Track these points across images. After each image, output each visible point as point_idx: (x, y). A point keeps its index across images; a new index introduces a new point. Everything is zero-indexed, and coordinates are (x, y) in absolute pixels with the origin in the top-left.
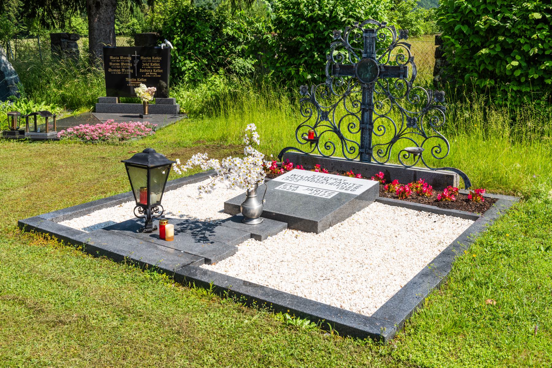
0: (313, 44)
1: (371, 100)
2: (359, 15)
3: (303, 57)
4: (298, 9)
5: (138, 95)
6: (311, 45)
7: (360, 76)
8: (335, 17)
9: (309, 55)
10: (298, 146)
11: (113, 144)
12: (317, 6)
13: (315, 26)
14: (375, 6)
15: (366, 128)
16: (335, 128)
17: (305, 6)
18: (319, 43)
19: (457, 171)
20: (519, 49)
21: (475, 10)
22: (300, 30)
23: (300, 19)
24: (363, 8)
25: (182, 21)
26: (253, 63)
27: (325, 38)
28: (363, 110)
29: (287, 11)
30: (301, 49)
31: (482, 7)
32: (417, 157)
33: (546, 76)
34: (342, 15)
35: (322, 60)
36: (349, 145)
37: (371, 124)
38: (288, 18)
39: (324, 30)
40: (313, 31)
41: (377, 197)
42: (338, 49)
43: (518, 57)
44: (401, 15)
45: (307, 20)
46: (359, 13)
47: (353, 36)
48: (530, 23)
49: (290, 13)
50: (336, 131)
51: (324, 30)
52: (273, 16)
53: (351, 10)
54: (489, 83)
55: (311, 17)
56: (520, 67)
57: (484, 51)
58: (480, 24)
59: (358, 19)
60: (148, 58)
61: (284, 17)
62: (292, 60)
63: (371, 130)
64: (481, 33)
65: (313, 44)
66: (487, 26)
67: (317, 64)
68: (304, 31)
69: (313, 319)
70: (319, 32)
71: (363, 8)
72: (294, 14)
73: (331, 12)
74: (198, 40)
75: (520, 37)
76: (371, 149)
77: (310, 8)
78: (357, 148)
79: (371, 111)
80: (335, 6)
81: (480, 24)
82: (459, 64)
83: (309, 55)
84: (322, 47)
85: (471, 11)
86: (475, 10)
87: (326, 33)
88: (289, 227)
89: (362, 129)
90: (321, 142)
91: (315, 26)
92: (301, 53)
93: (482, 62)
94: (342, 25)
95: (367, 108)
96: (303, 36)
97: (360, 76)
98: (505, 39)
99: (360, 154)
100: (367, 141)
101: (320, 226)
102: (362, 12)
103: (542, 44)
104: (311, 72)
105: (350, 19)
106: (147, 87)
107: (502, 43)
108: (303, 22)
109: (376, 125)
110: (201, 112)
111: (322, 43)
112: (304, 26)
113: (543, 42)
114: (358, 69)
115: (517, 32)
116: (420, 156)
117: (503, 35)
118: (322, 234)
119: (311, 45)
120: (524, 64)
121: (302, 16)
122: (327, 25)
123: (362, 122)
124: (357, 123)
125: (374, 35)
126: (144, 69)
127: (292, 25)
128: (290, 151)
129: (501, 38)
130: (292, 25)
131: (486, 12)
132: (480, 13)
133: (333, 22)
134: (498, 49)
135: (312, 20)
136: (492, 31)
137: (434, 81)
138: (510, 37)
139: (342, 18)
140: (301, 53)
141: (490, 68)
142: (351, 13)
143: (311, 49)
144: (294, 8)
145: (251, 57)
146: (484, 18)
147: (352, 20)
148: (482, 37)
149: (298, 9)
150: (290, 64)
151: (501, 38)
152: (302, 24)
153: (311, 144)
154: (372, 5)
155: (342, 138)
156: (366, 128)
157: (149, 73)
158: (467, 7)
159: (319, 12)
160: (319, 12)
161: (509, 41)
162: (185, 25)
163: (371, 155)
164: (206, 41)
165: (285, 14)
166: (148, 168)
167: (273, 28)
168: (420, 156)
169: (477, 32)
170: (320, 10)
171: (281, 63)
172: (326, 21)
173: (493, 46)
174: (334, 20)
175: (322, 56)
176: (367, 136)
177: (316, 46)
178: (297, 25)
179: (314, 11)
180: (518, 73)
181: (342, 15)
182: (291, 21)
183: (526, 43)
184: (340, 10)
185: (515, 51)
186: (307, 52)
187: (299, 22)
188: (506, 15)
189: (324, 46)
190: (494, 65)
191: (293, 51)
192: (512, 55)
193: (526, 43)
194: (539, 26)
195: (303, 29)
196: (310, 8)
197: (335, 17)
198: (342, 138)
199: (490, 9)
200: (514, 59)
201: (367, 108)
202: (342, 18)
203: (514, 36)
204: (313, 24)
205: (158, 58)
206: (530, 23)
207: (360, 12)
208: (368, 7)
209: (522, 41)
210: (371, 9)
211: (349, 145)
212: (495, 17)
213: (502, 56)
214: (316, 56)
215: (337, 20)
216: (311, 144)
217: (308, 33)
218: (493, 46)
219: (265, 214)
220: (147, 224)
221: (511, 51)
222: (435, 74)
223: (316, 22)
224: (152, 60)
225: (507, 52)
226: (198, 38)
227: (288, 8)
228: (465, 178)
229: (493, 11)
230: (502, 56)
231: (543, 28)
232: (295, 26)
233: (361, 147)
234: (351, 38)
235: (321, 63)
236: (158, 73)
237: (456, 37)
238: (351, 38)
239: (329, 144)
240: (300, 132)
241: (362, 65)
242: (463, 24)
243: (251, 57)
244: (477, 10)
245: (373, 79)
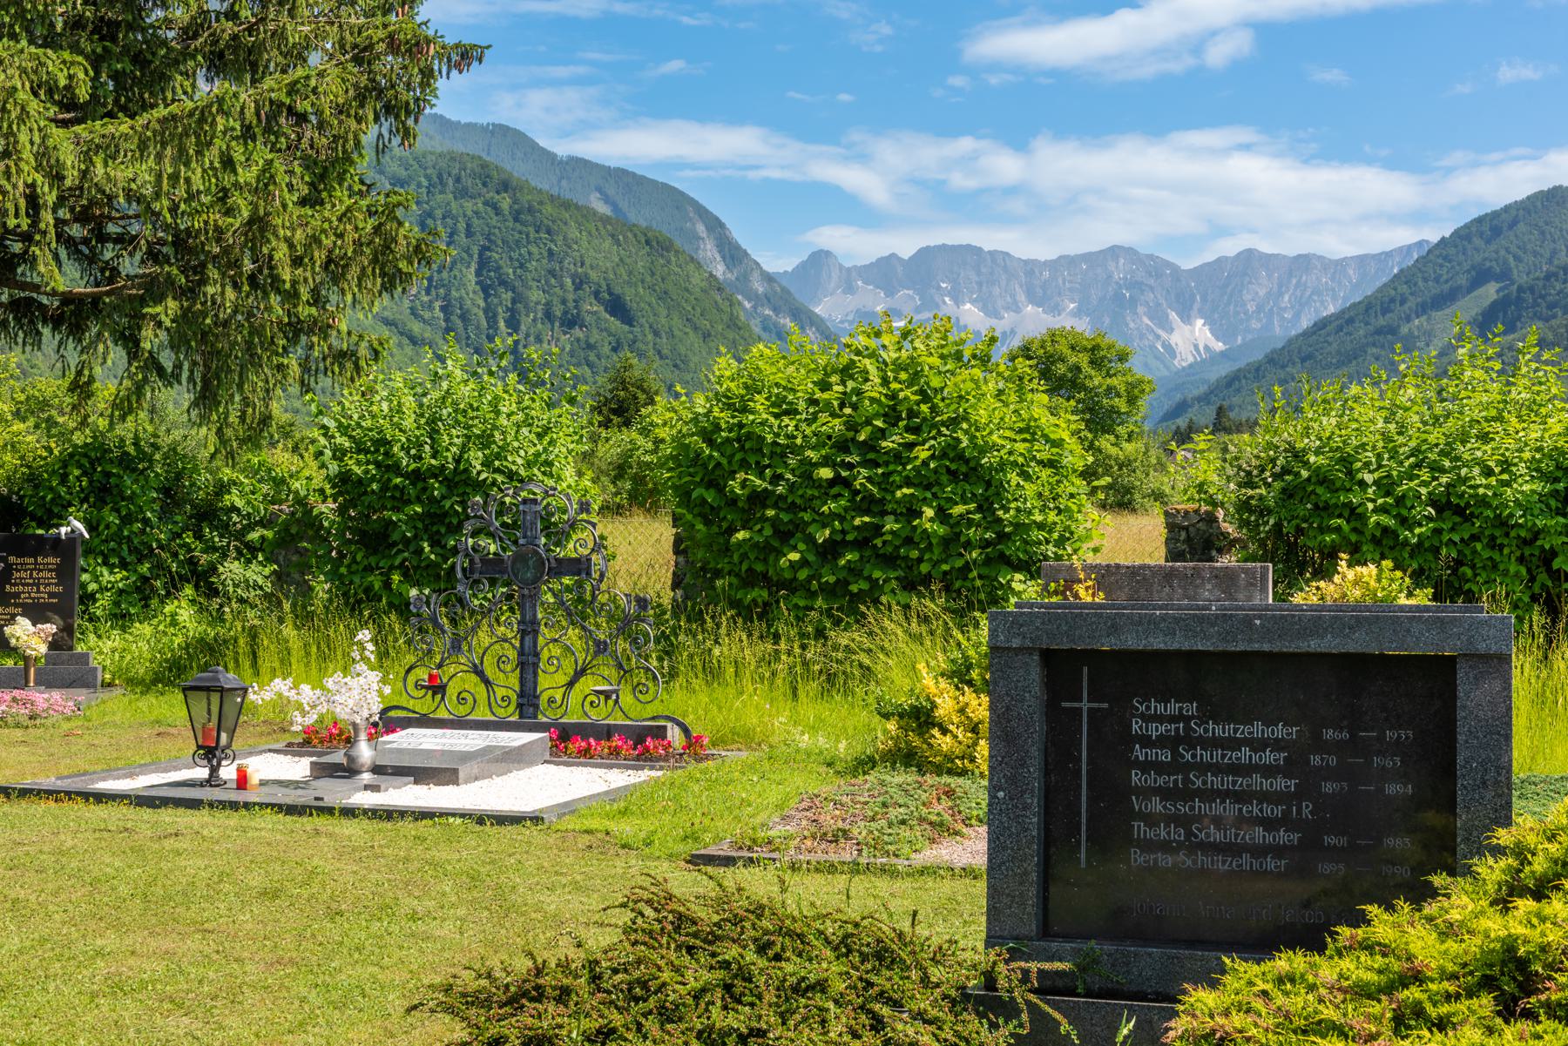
0: (420, 525)
1: (535, 615)
2: (514, 468)
3: (400, 552)
4: (386, 454)
5: (13, 642)
6: (415, 527)
7: (516, 576)
8: (466, 470)
9: (412, 549)
10: (411, 704)
11: (18, 725)
12: (427, 448)
13: (425, 489)
14: (545, 450)
15: (528, 663)
16: (475, 665)
17: (402, 448)
18: (433, 524)
19: (668, 718)
20: (803, 532)
21: (724, 461)
22: (393, 497)
23: (391, 475)
24: (522, 453)
25: (85, 473)
26: (267, 571)
27: (446, 514)
28: (523, 633)
29: (361, 456)
30: (395, 537)
31: (738, 456)
32: (611, 703)
33: (851, 579)
34: (479, 468)
35: (440, 560)
36: (500, 692)
37: (537, 655)
38: (367, 472)
39: (444, 497)
40: (419, 500)
41: (547, 757)
42: (474, 534)
43: (801, 546)
44: (650, 446)
45: (406, 476)
46: (514, 463)
47: (502, 510)
48: (820, 486)
49: (368, 463)
50: (478, 671)
51: (444, 497)
52: (334, 468)
53: (498, 457)
54: (760, 594)
55: (416, 471)
56: (804, 563)
57: (741, 535)
58: (734, 485)
59: (511, 475)
60: (28, 560)
61: (358, 470)
62: (373, 560)
63: (536, 665)
64: (740, 504)
65: (420, 525)
66: (746, 492)
67: (428, 566)
68: (401, 501)
69: (463, 816)
70: (432, 499)
71: (522, 453)
72: (378, 465)
73: (458, 461)
74: (127, 520)
75: (805, 510)
76: (538, 697)
77: (413, 452)
78: (514, 697)
79: (536, 632)
80: (464, 448)
81: (734, 485)
82: (706, 563)
83: (412, 549)
84: (438, 532)
85: (719, 464)
86: (724, 461)
87: (447, 504)
88: (416, 782)
89: (522, 665)
90: (452, 691)
91: (425, 489)
92: (395, 544)
93: (744, 556)
94: (480, 486)
95: (529, 629)
96: (397, 509)
97: (516, 576)
98: (777, 515)
99: (520, 706)
100: (529, 685)
101: (461, 775)
102: (520, 461)
103: (841, 523)
104: (417, 584)
105: (496, 476)
106: (34, 625)
107: (774, 522)
108: (398, 480)
109: (545, 655)
110: (155, 682)
111: (439, 524)
112: (402, 490)
113: (842, 519)
114: (514, 562)
115: (798, 501)
116: (616, 701)
117: (775, 506)
118: (463, 787)
119: (415, 527)
120: (811, 558)
121: (396, 469)
122: (449, 487)
123: (521, 653)
124: (512, 655)
125: (538, 508)
126: (15, 585)
127: (374, 486)
128: (392, 714)
129: (770, 513)
130: (374, 486)
131: (745, 465)
132: (736, 467)
133: (460, 481)
134: (768, 532)
135: (416, 476)
136: (758, 499)
137: (674, 600)
138: (787, 510)
139: (479, 473)
140: (395, 544)
141: (759, 567)
142: (497, 463)
143: (415, 536)
144: (377, 451)
145: (260, 558)
146: (740, 476)
147: (500, 478)
148: (743, 510)
149: (386, 454)
150: (369, 569)
151: (770, 513)
152: (396, 486)
153: (434, 694)
154: (540, 448)
155: (487, 682)
156: (528, 663)
157: (28, 595)
158: (711, 456)
159: (433, 462)
160: (433, 462)
161: (785, 517)
162: (91, 482)
163: (536, 707)
164: (146, 522)
165: (358, 463)
166: (222, 690)
167: (329, 492)
168: (616, 701)
169: (733, 502)
170: (434, 457)
171: (349, 566)
172: (446, 479)
173: (758, 527)
174: (464, 477)
175: (438, 550)
176: (530, 677)
177: (426, 529)
178: (385, 487)
179: (420, 458)
180: (803, 575)
181: (479, 468)
182: (373, 479)
183: (814, 520)
184: (476, 458)
185: (799, 535)
186: (407, 542)
187: (389, 480)
188: (779, 471)
189: (443, 530)
190: (765, 560)
191: (376, 540)
192: (792, 542)
193: (814, 520)
194: (834, 491)
195: (398, 495)
196: (413, 452)
197: (466, 470)
198: (487, 682)
199: (752, 460)
200: (794, 548)
201: (529, 629)
202: (479, 473)
203: (793, 508)
204: (420, 485)
205: (51, 560)
206: (820, 486)
207: (516, 462)
208: (532, 451)
209: (807, 517)
210: (537, 455)
211: (500, 692)
212: (761, 475)
213: (776, 544)
214: (427, 549)
215: (469, 478)
216: (434, 694)
217: (409, 502)
218: (758, 527)
219: (377, 770)
220: (213, 781)
221: (791, 534)
222: (675, 585)
223: (424, 480)
224: (36, 563)
225: (784, 536)
226: (129, 514)
227: (367, 452)
228: (686, 730)
229: (758, 463)
230: (776, 544)
231: (840, 495)
232: (381, 490)
233: (521, 695)
234: (500, 514)
235: (436, 565)
236: (51, 595)
237: (696, 511)
238: (500, 514)
239: (464, 695)
240: (411, 678)
241: (519, 558)
242: (707, 488)
243: (260, 558)
244: (730, 462)
245: (537, 580)
